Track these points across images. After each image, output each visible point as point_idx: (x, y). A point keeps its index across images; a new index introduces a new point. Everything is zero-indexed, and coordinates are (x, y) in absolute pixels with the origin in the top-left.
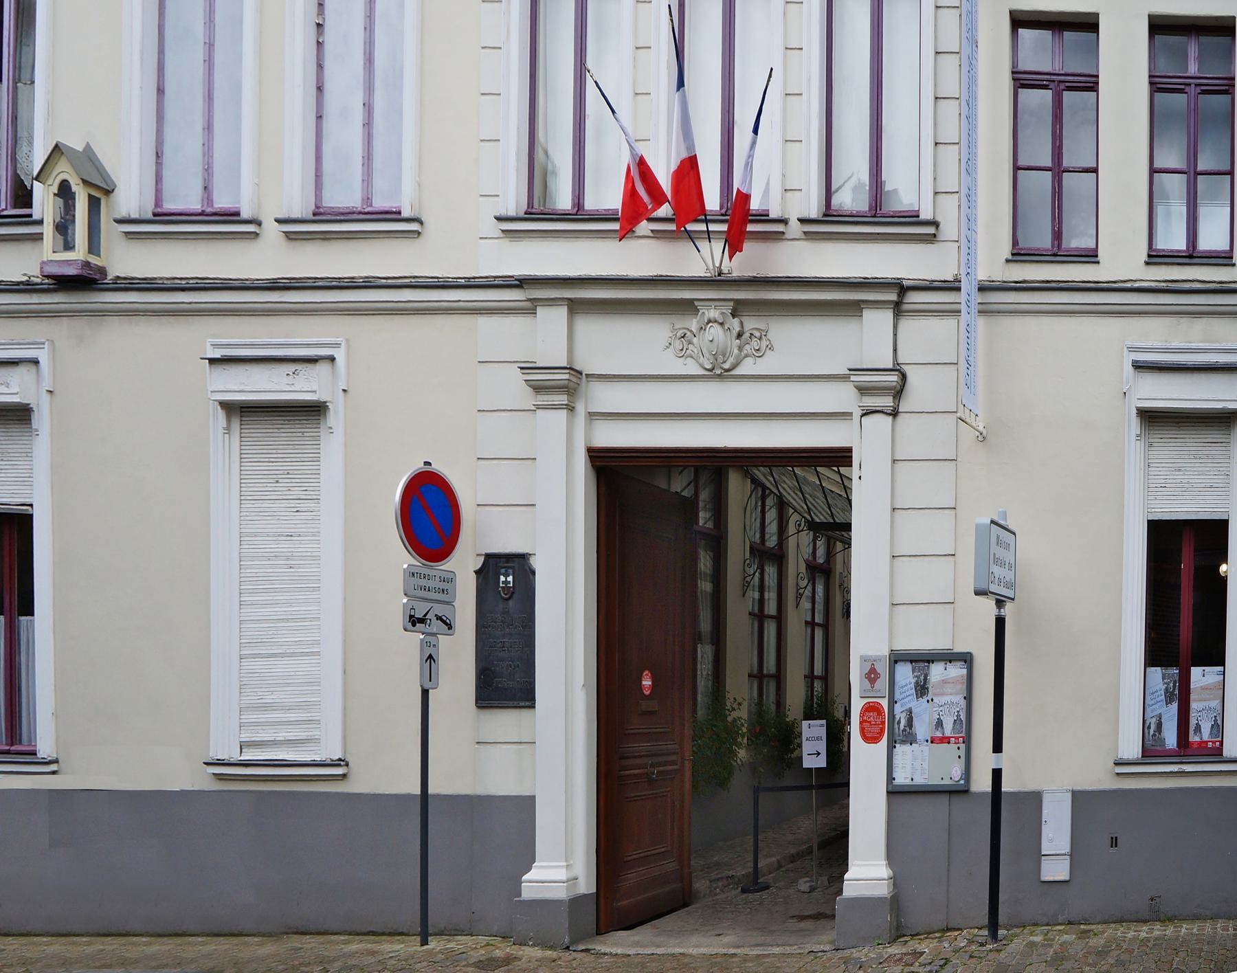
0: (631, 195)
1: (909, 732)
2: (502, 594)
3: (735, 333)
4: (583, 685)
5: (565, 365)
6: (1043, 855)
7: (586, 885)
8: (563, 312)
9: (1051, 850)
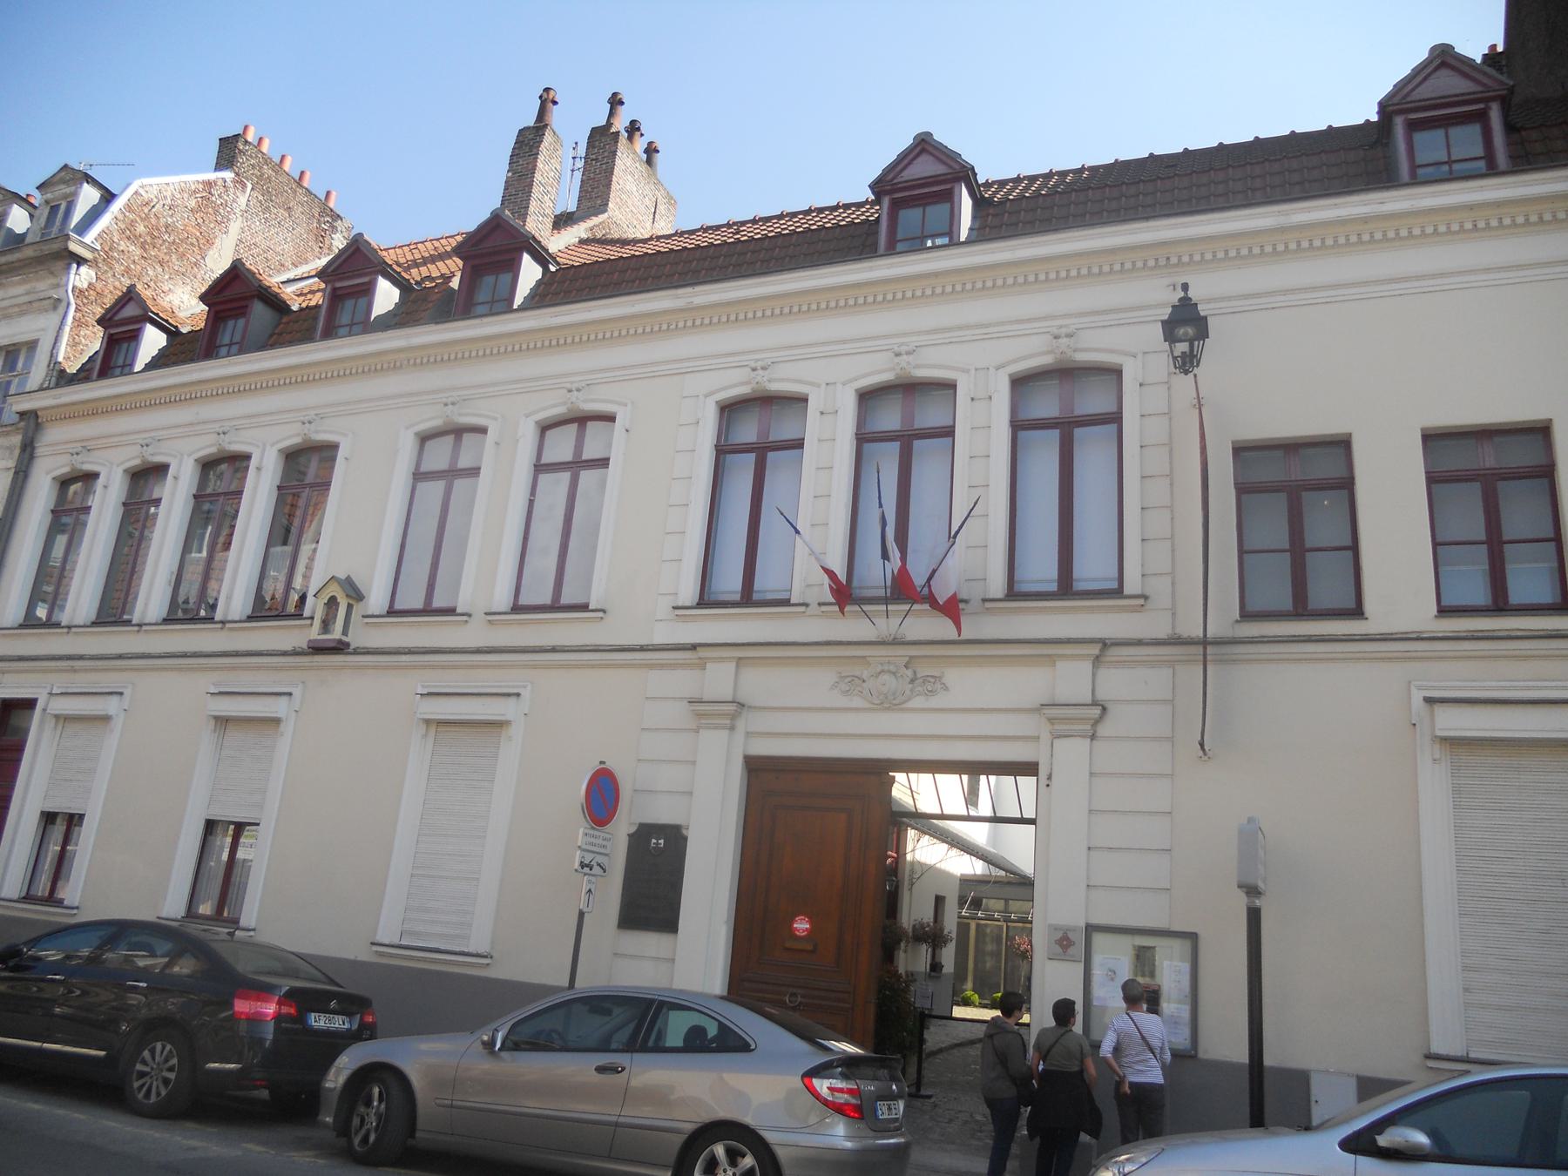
5: (731, 700)
8: (732, 666)
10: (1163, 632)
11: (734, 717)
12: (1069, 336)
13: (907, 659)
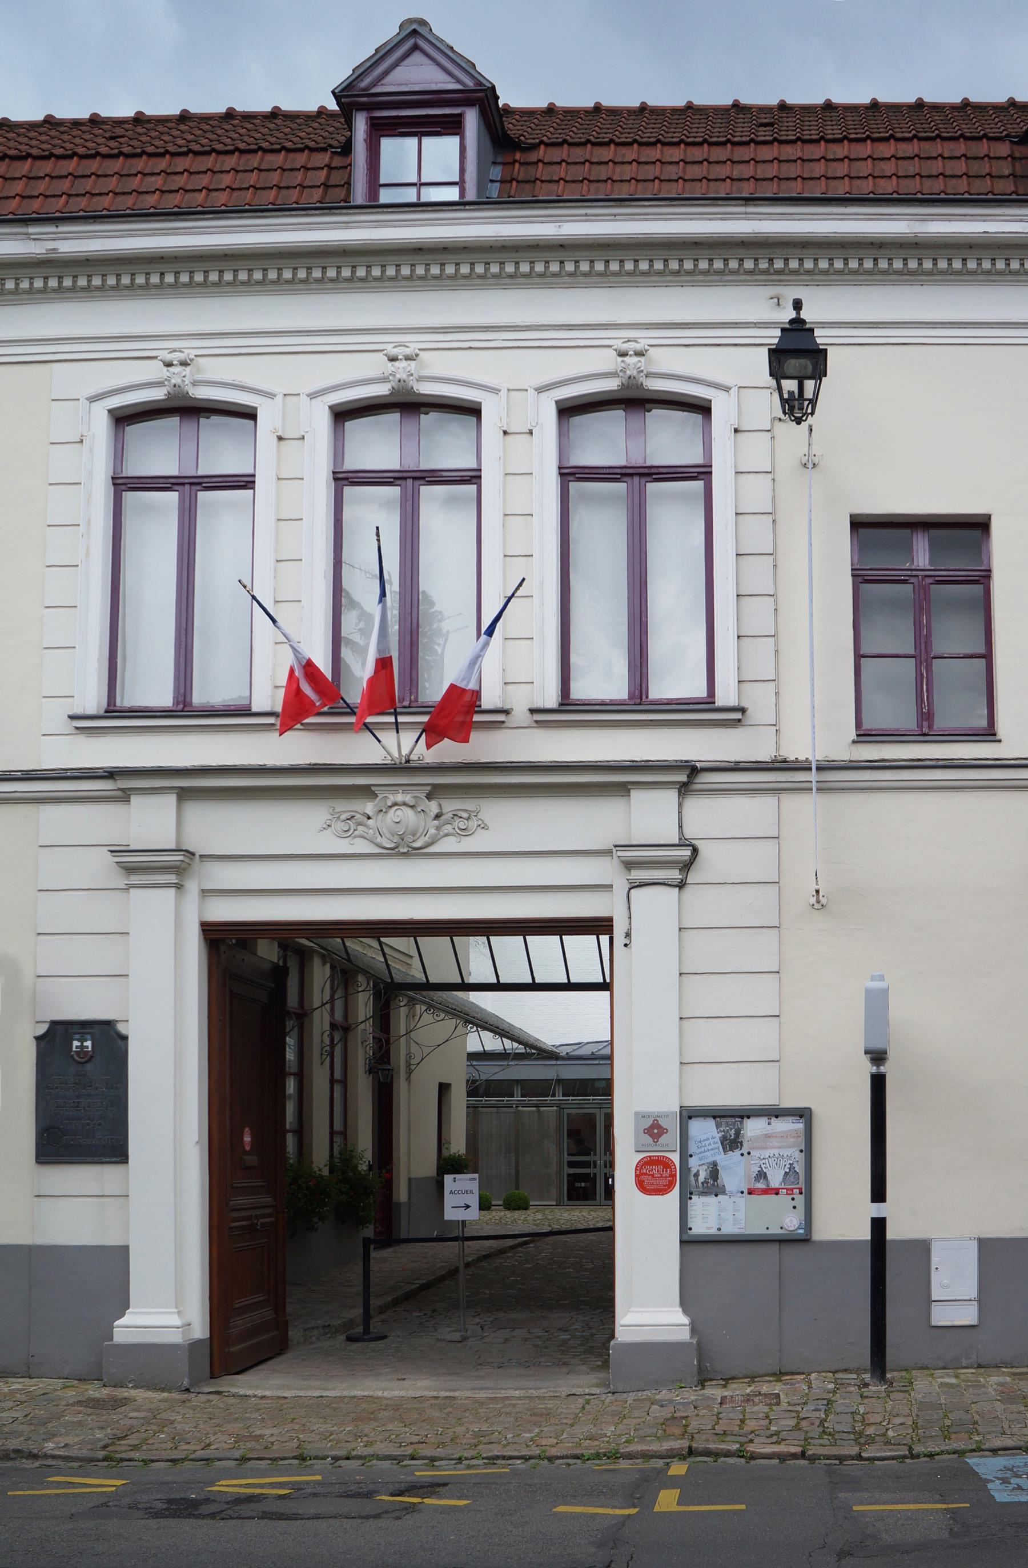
0: (294, 693)
1: (714, 1185)
2: (77, 1058)
3: (433, 814)
4: (197, 1142)
5: (173, 847)
6: (934, 1301)
7: (200, 1330)
8: (172, 799)
9: (945, 1296)
10: (765, 754)
11: (179, 870)
12: (639, 354)
13: (429, 788)
